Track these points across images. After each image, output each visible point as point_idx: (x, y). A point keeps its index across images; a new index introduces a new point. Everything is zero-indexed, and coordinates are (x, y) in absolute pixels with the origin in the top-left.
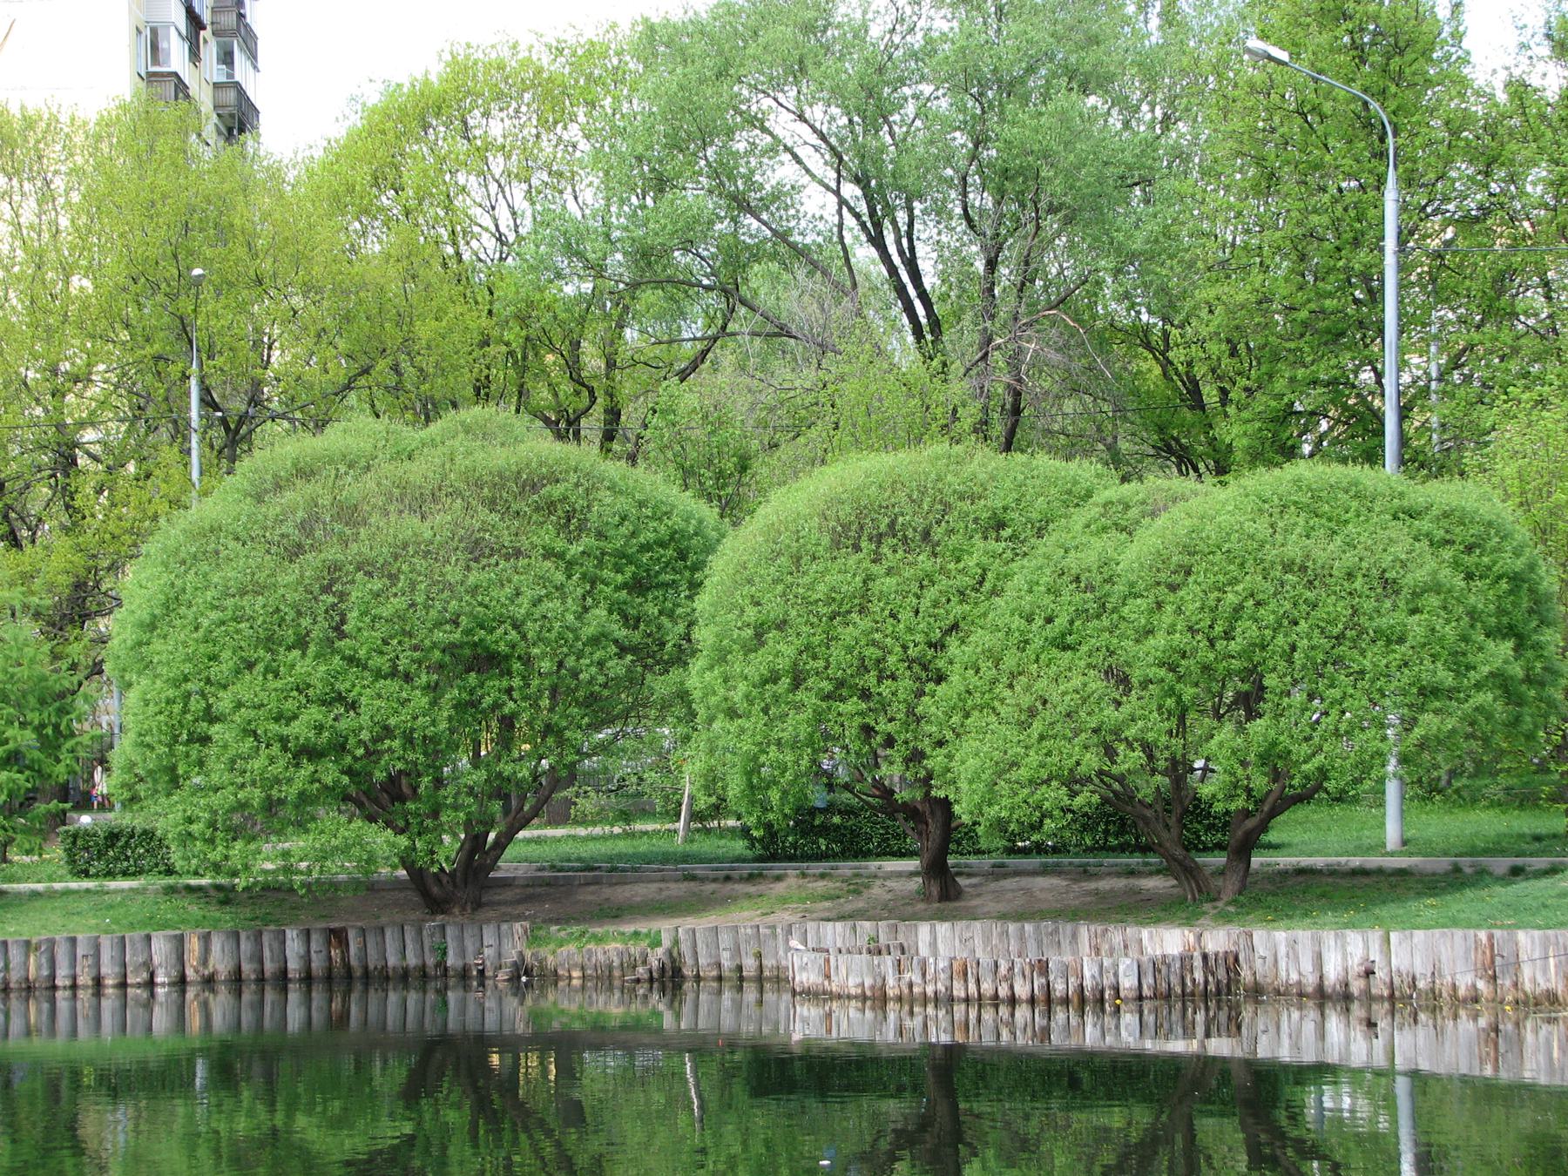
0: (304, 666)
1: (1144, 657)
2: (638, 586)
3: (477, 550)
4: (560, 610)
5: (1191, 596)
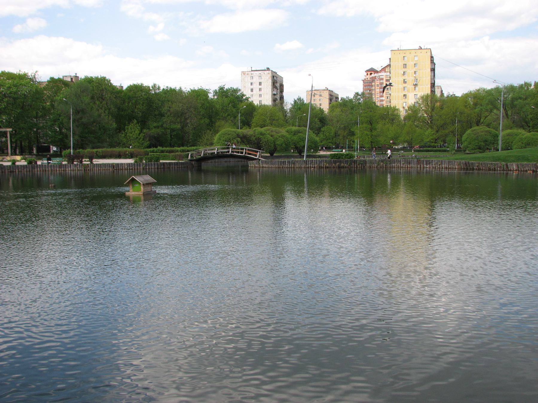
0: (476, 141)
1: (524, 142)
2: (494, 137)
3: (486, 135)
4: (490, 138)
5: (526, 140)
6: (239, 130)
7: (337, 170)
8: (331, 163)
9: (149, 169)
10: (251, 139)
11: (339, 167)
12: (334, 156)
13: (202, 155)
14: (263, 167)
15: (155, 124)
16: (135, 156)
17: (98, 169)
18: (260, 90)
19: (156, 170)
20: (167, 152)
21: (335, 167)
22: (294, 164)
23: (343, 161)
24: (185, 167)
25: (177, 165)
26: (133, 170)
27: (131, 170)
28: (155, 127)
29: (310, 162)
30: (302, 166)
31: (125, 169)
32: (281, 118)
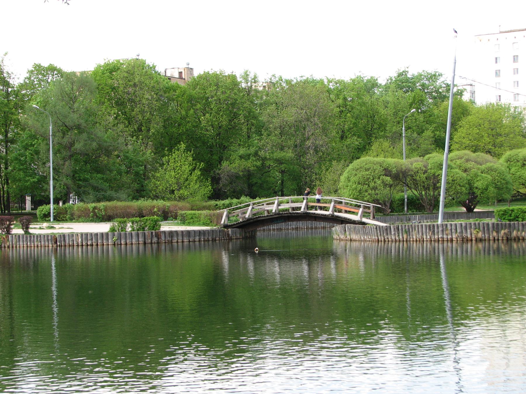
6: (404, 160)
7: (502, 246)
8: (488, 229)
9: (126, 244)
10: (418, 178)
11: (509, 240)
12: (503, 214)
13: (247, 216)
14: (351, 240)
15: (242, 151)
16: (172, 216)
17: (27, 244)
18: (516, 71)
19: (141, 247)
20: (351, 205)
21: (498, 240)
22: (408, 232)
23: (516, 225)
24: (208, 241)
25: (189, 236)
26: (94, 247)
27: (89, 247)
28: (241, 157)
29: (440, 229)
30: (425, 237)
31: (78, 246)
32: (433, 132)
